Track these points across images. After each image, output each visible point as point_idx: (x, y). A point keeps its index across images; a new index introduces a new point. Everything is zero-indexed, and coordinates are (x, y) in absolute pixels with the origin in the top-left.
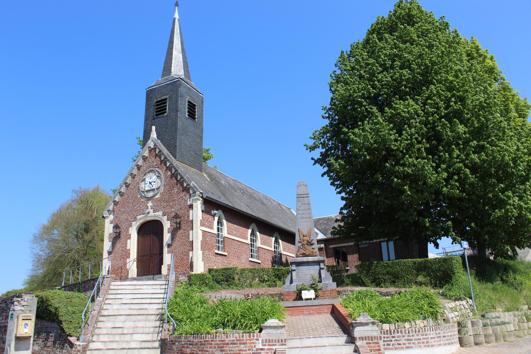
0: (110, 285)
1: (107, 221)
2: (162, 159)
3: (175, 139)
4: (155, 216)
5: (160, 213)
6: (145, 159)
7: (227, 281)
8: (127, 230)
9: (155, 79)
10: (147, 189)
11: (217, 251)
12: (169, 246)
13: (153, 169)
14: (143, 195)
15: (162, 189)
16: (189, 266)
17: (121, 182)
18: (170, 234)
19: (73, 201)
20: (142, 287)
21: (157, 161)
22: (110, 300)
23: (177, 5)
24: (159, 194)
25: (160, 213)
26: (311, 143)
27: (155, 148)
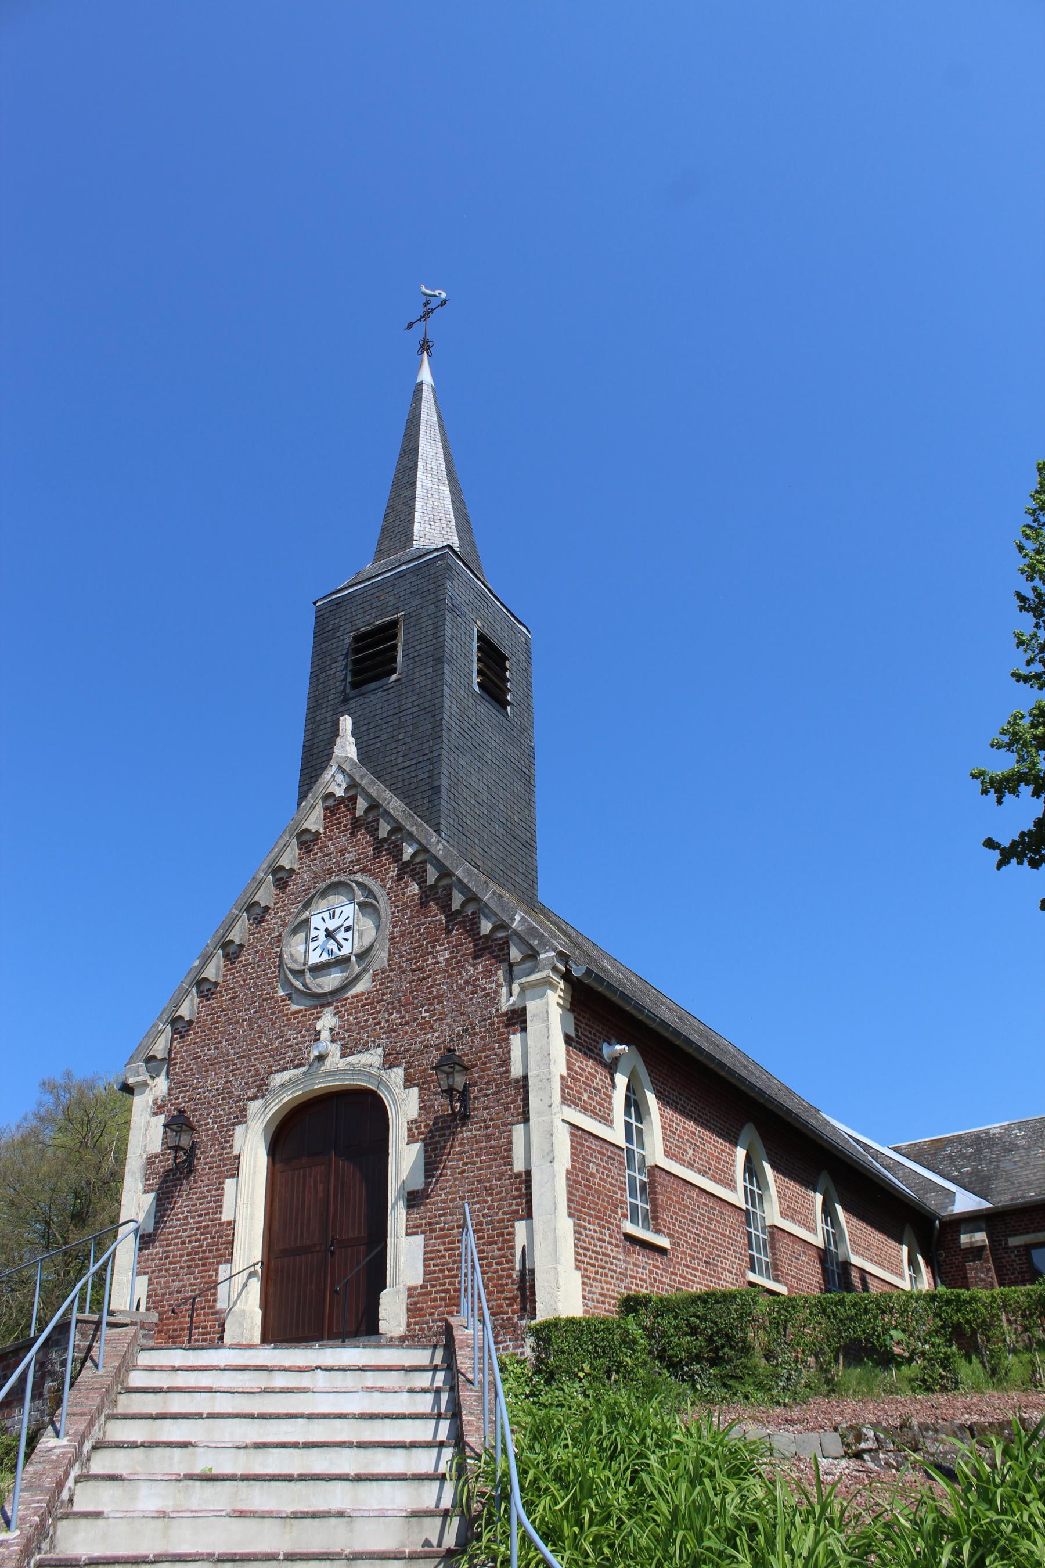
0: (127, 1365)
1: (141, 1104)
2: (383, 834)
3: (434, 762)
4: (352, 1070)
5: (373, 1058)
6: (307, 841)
7: (714, 1362)
8: (226, 1138)
9: (350, 563)
10: (314, 959)
11: (629, 1228)
12: (414, 1199)
13: (344, 878)
14: (299, 985)
15: (381, 957)
16: (513, 1290)
17: (208, 940)
18: (417, 1147)
19: (42, 1119)
20: (304, 1380)
21: (356, 848)
22: (121, 1454)
23: (425, 346)
24: (367, 977)
25: (373, 1058)
26: (1005, 763)
27: (353, 799)
